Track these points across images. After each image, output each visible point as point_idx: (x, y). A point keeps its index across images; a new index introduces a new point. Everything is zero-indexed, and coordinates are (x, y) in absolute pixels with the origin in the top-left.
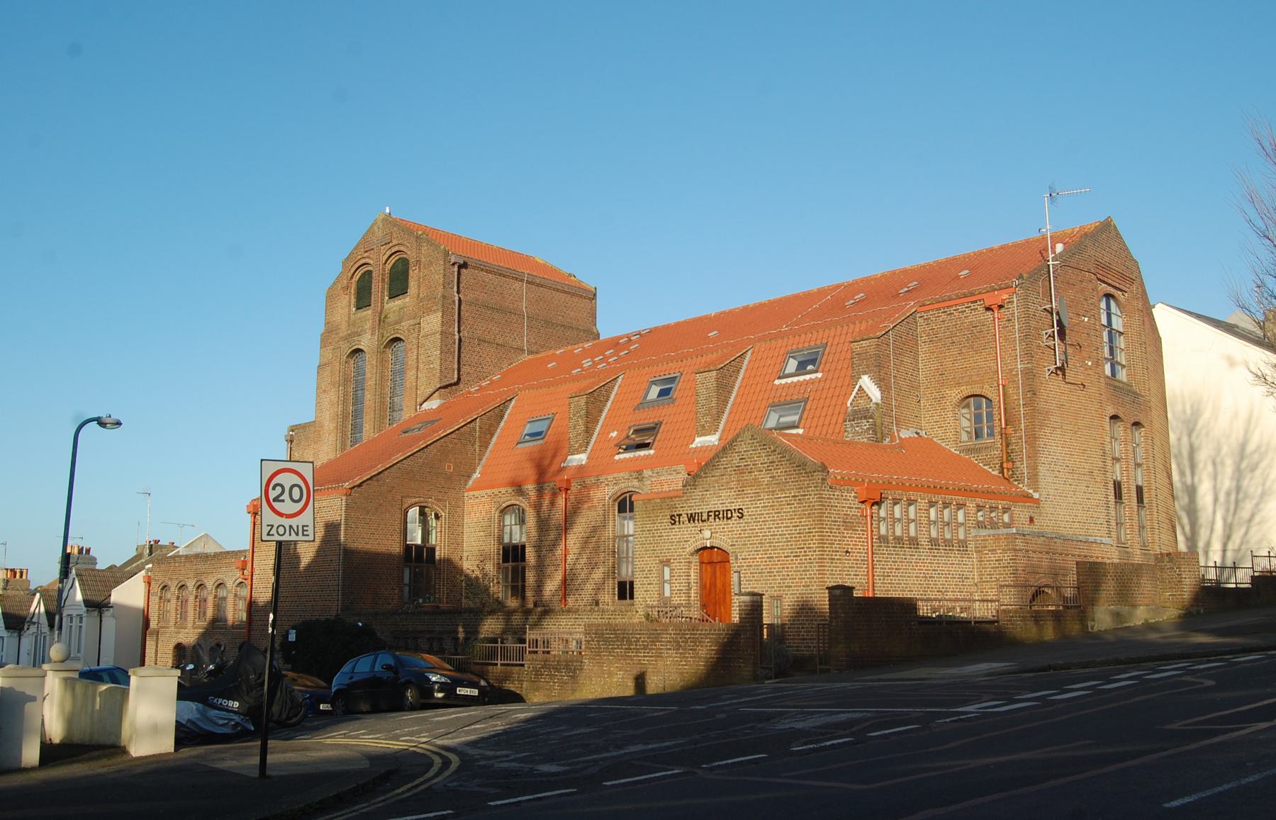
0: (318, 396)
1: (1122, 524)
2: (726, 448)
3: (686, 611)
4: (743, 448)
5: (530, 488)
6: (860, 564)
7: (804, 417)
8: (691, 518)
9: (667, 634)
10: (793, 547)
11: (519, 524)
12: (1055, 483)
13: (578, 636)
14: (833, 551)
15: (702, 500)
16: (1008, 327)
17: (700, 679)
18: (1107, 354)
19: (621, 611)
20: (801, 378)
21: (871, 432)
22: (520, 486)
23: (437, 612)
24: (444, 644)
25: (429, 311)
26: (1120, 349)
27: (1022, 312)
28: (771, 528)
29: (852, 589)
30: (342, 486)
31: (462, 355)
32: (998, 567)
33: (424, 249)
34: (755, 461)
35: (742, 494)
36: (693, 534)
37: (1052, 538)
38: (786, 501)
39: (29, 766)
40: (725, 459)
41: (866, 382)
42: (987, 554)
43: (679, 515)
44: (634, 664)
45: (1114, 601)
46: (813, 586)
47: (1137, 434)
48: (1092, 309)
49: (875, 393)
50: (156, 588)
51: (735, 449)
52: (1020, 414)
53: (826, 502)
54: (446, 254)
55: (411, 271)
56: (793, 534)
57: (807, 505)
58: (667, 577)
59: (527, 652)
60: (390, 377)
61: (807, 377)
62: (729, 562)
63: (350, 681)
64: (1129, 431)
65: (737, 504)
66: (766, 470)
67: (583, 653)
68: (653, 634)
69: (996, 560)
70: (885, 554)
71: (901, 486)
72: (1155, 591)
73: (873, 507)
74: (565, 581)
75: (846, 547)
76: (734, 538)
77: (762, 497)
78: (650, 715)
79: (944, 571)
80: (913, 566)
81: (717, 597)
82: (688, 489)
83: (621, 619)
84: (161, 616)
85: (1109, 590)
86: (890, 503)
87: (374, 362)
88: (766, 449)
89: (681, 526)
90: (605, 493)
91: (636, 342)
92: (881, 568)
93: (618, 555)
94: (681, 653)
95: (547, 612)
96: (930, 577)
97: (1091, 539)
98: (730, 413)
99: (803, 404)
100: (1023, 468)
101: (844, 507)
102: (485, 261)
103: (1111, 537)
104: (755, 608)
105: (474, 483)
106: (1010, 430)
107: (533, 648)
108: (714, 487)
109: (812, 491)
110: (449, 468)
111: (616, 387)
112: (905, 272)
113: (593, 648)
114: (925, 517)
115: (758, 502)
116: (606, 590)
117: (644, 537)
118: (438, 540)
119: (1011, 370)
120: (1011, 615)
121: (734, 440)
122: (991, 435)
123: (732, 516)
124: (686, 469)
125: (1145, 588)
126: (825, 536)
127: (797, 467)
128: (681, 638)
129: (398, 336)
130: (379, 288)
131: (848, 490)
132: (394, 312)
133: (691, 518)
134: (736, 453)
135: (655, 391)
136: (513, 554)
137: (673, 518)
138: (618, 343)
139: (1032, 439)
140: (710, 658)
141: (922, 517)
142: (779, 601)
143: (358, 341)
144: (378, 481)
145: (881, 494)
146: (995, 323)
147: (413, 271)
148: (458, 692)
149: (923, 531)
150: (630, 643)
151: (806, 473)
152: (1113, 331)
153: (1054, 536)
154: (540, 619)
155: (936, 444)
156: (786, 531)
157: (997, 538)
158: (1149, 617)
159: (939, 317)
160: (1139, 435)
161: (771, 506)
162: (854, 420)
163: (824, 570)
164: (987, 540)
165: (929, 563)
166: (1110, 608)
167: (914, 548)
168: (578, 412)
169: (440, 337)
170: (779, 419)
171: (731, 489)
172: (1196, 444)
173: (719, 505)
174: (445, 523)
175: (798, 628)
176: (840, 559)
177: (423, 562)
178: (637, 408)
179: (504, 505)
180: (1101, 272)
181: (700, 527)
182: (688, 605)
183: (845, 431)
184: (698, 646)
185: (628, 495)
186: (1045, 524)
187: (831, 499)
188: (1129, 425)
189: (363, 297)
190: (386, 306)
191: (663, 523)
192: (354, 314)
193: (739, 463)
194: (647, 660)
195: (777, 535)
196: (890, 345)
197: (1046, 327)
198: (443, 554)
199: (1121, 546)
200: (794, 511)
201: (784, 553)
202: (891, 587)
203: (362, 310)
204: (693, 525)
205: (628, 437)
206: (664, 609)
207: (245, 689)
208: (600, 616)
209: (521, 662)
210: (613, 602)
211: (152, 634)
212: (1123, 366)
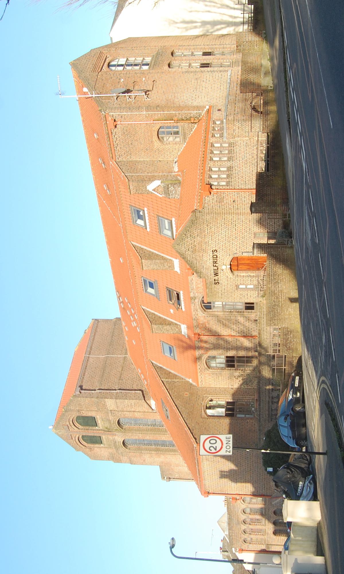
0: (146, 464)
1: (221, 64)
2: (183, 257)
3: (260, 278)
4: (184, 249)
5: (198, 353)
6: (240, 195)
7: (166, 217)
8: (216, 274)
9: (271, 287)
10: (231, 227)
11: (216, 359)
12: (201, 97)
13: (272, 330)
14: (234, 208)
15: (207, 269)
16: (125, 118)
17: (292, 272)
18: (137, 68)
19: (260, 309)
20: (147, 218)
21: (175, 186)
22: (197, 358)
23: (259, 400)
24: (275, 396)
25: (104, 405)
26: (135, 60)
27: (118, 110)
28: (222, 237)
29: (252, 203)
30: (196, 448)
31: (128, 388)
32: (242, 129)
33: (72, 408)
34: (190, 244)
35: (206, 251)
36: (224, 274)
37: (228, 101)
38: (209, 230)
39: (324, 561)
40: (188, 258)
41: (151, 187)
42: (235, 133)
43: (215, 280)
44: (285, 303)
45: (259, 75)
46: (250, 218)
47: (177, 54)
48: (116, 75)
49: (157, 183)
50: (245, 546)
51: (184, 253)
52: (168, 113)
53: (210, 211)
54: (75, 396)
55: (83, 415)
56: (225, 227)
57: (211, 220)
58: (244, 287)
59: (279, 354)
60: (138, 426)
61: (146, 215)
62: (237, 257)
63: (292, 438)
64: (176, 58)
65: (210, 253)
66: (194, 239)
67: (280, 327)
68: (271, 294)
69: (239, 129)
70: (235, 183)
71: (203, 174)
72: (254, 54)
73: (213, 188)
74: (244, 336)
75: (231, 202)
76: (226, 255)
77: (207, 241)
78: (306, 298)
79: (243, 155)
80: (241, 170)
81: (254, 263)
82: (202, 276)
83: (264, 308)
84: (259, 543)
85: (254, 78)
86: (211, 180)
87: (130, 434)
88: (184, 239)
89: (220, 279)
90: (201, 316)
91: (123, 299)
92: (242, 185)
93: (232, 310)
94: (280, 281)
95: (260, 345)
96: (246, 161)
97: (229, 81)
98: (163, 253)
99: (160, 218)
100: (194, 113)
101: (213, 202)
102: (78, 376)
103: (228, 70)
104: (261, 247)
105: (194, 382)
106: (175, 118)
107: (277, 351)
108: (202, 263)
109: (205, 217)
110: (187, 394)
111: (148, 309)
112: (92, 164)
113: (278, 322)
114: (217, 163)
115: (209, 242)
116: (249, 316)
117: (225, 297)
118: (222, 400)
119: (146, 117)
120: (265, 127)
121: (179, 253)
122: (177, 127)
123: (216, 255)
124: (191, 275)
125: (252, 59)
126: (226, 212)
127: (193, 224)
128: (273, 281)
129: (117, 421)
130: (91, 432)
131: (204, 200)
132: (104, 424)
133: (216, 274)
134: (185, 253)
135: (150, 290)
136: (231, 362)
137: (216, 283)
138: (124, 308)
139: (180, 108)
140: (283, 268)
141: (217, 165)
142: (257, 234)
143: (119, 442)
144: (193, 430)
145: (206, 184)
146: (123, 124)
147: (83, 414)
148: (297, 386)
149: (224, 164)
150: (275, 305)
151: (196, 220)
152: (126, 64)
153: (227, 100)
154: (263, 348)
155: (181, 154)
156: (223, 230)
157: (228, 128)
158: (267, 59)
159: (118, 150)
160: (177, 53)
161: (211, 236)
162: (169, 194)
163: (242, 213)
164: (229, 133)
165: (239, 161)
166: (262, 78)
167: (232, 169)
168: (160, 329)
169: (118, 400)
170: (167, 230)
171: (203, 255)
172: (181, 20)
173: (210, 261)
174: (214, 396)
175: (269, 225)
176: (237, 205)
177: (234, 408)
178: (159, 299)
179: (206, 366)
180: (97, 69)
181: (220, 270)
182: (258, 276)
183: (174, 198)
184: (277, 273)
185: (202, 305)
186: (221, 103)
187: (209, 208)
188: (173, 58)
189: (96, 440)
190: (101, 428)
191: (218, 288)
192: (104, 445)
193: (190, 251)
194: (283, 297)
195: (225, 235)
196: (132, 175)
197: (125, 99)
198: (230, 398)
199: (232, 64)
200: (214, 226)
201: (234, 231)
202: (251, 180)
203: (102, 441)
204: (219, 274)
205: (173, 304)
206: (259, 288)
207: (294, 479)
208: (262, 319)
209: (284, 357)
210: (255, 312)
211: (268, 548)
212: (144, 59)
